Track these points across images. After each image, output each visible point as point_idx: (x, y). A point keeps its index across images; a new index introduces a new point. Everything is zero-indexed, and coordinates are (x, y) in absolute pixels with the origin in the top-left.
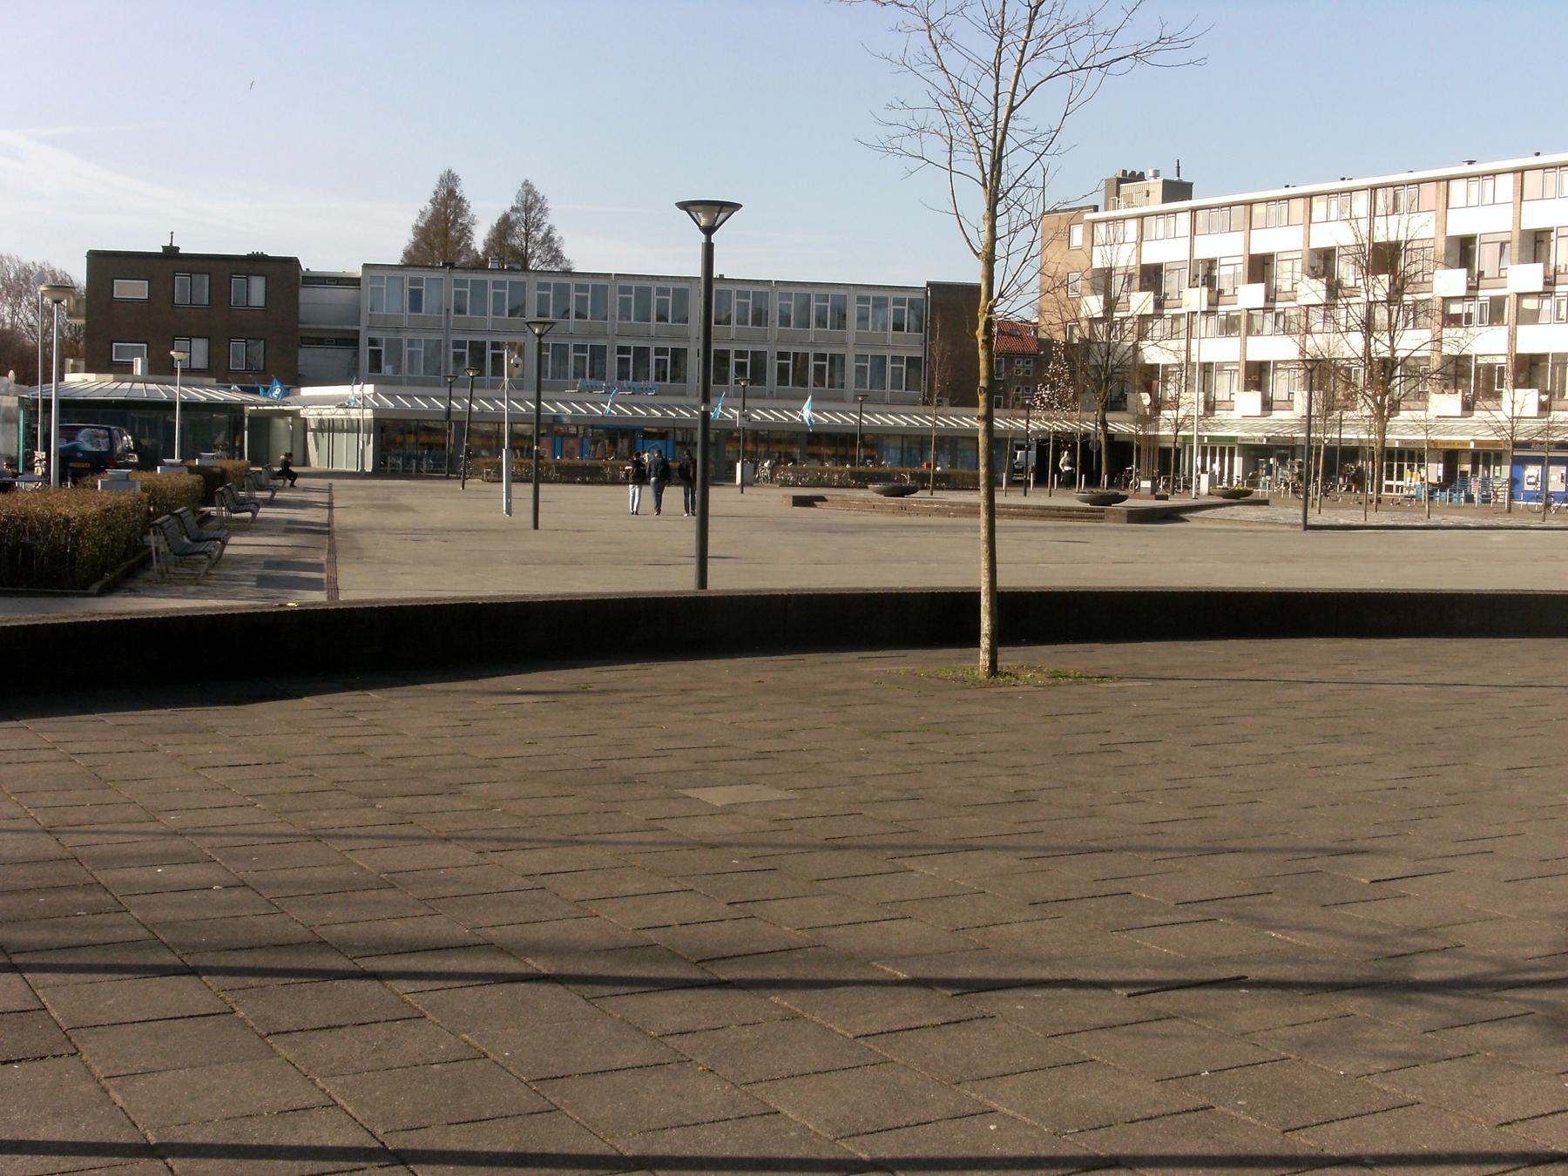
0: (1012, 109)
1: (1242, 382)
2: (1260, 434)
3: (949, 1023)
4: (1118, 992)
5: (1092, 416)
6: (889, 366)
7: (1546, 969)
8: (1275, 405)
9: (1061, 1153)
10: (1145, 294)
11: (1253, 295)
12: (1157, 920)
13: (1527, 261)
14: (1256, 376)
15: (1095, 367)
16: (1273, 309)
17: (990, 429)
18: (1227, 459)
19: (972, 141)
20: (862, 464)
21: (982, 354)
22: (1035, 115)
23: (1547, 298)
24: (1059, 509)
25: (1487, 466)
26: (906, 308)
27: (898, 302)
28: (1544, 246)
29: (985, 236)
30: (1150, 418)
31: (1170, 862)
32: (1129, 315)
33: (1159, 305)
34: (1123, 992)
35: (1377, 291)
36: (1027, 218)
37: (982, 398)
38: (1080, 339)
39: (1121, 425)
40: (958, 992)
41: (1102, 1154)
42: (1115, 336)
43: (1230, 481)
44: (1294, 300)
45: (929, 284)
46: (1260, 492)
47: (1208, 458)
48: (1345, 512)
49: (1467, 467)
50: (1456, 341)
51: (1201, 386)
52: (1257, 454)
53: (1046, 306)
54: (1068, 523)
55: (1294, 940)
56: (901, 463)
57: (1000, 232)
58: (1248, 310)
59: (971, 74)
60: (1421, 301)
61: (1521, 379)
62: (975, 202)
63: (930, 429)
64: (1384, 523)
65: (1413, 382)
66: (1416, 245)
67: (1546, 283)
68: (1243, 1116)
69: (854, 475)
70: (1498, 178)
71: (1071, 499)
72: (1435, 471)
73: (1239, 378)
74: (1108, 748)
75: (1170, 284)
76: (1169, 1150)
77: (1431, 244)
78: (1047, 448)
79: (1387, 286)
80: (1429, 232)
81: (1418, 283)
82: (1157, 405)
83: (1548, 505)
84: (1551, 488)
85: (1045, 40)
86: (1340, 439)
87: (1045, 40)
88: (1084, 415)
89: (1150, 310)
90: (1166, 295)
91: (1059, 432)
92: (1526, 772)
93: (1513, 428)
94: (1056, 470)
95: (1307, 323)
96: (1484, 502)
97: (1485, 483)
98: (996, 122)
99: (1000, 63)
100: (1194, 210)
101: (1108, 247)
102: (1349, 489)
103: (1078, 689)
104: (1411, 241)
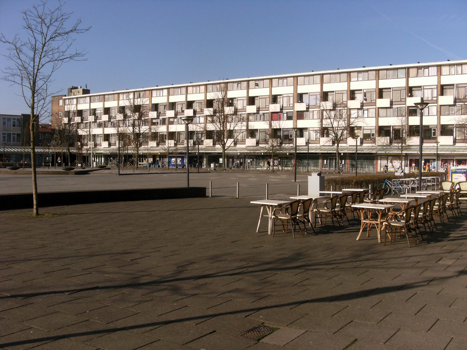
0: (38, 70)
1: (103, 139)
2: (108, 152)
3: (21, 306)
4: (66, 293)
5: (66, 148)
6: (12, 136)
7: (171, 277)
8: (112, 145)
9: (50, 336)
10: (78, 117)
11: (105, 118)
12: (77, 274)
13: (3, 122)
14: (107, 137)
15: (66, 136)
16: (110, 121)
17: (34, 152)
18: (100, 158)
19: (28, 78)
20: (6, 161)
21: (31, 132)
22: (44, 71)
23: (175, 118)
24: (57, 172)
25: (163, 158)
26: (16, 121)
27: (13, 119)
28: (174, 106)
29: (32, 102)
30: (81, 149)
31: (81, 260)
32: (74, 122)
33: (82, 120)
34: (67, 293)
35: (135, 117)
36: (42, 98)
37: (32, 144)
38: (62, 129)
39: (73, 150)
40: (24, 298)
41: (60, 335)
42: (71, 128)
43: (101, 164)
44: (116, 119)
45: (22, 115)
46: (109, 166)
47: (96, 158)
48: (129, 170)
49: (158, 159)
50: (154, 129)
51: (93, 140)
52: (107, 157)
53: (53, 120)
54: (60, 175)
55: (111, 276)
56: (16, 161)
57: (35, 101)
58: (104, 121)
59: (28, 61)
60: (146, 119)
61: (170, 138)
62: (29, 93)
63: (23, 152)
64: (138, 173)
65: (145, 139)
66: (144, 106)
67: (175, 115)
68: (96, 321)
69: (3, 164)
70: (114, 95)
71: (60, 169)
72: (151, 160)
73: (102, 138)
74: (67, 232)
75: (85, 115)
76: (78, 332)
77: (148, 105)
78: (55, 156)
79: (138, 115)
80: (148, 103)
81: (145, 115)
82: (82, 145)
83: (177, 168)
84: (178, 163)
85: (47, 53)
86: (128, 153)
87: (47, 53)
88: (64, 148)
89: (80, 121)
90: (84, 117)
91: (57, 152)
92: (169, 231)
93: (168, 149)
94: (57, 162)
95: (119, 125)
96: (162, 167)
97: (163, 163)
98: (34, 73)
99: (35, 58)
100: (90, 97)
101: (69, 106)
102: (130, 165)
103: (60, 217)
104: (143, 105)
